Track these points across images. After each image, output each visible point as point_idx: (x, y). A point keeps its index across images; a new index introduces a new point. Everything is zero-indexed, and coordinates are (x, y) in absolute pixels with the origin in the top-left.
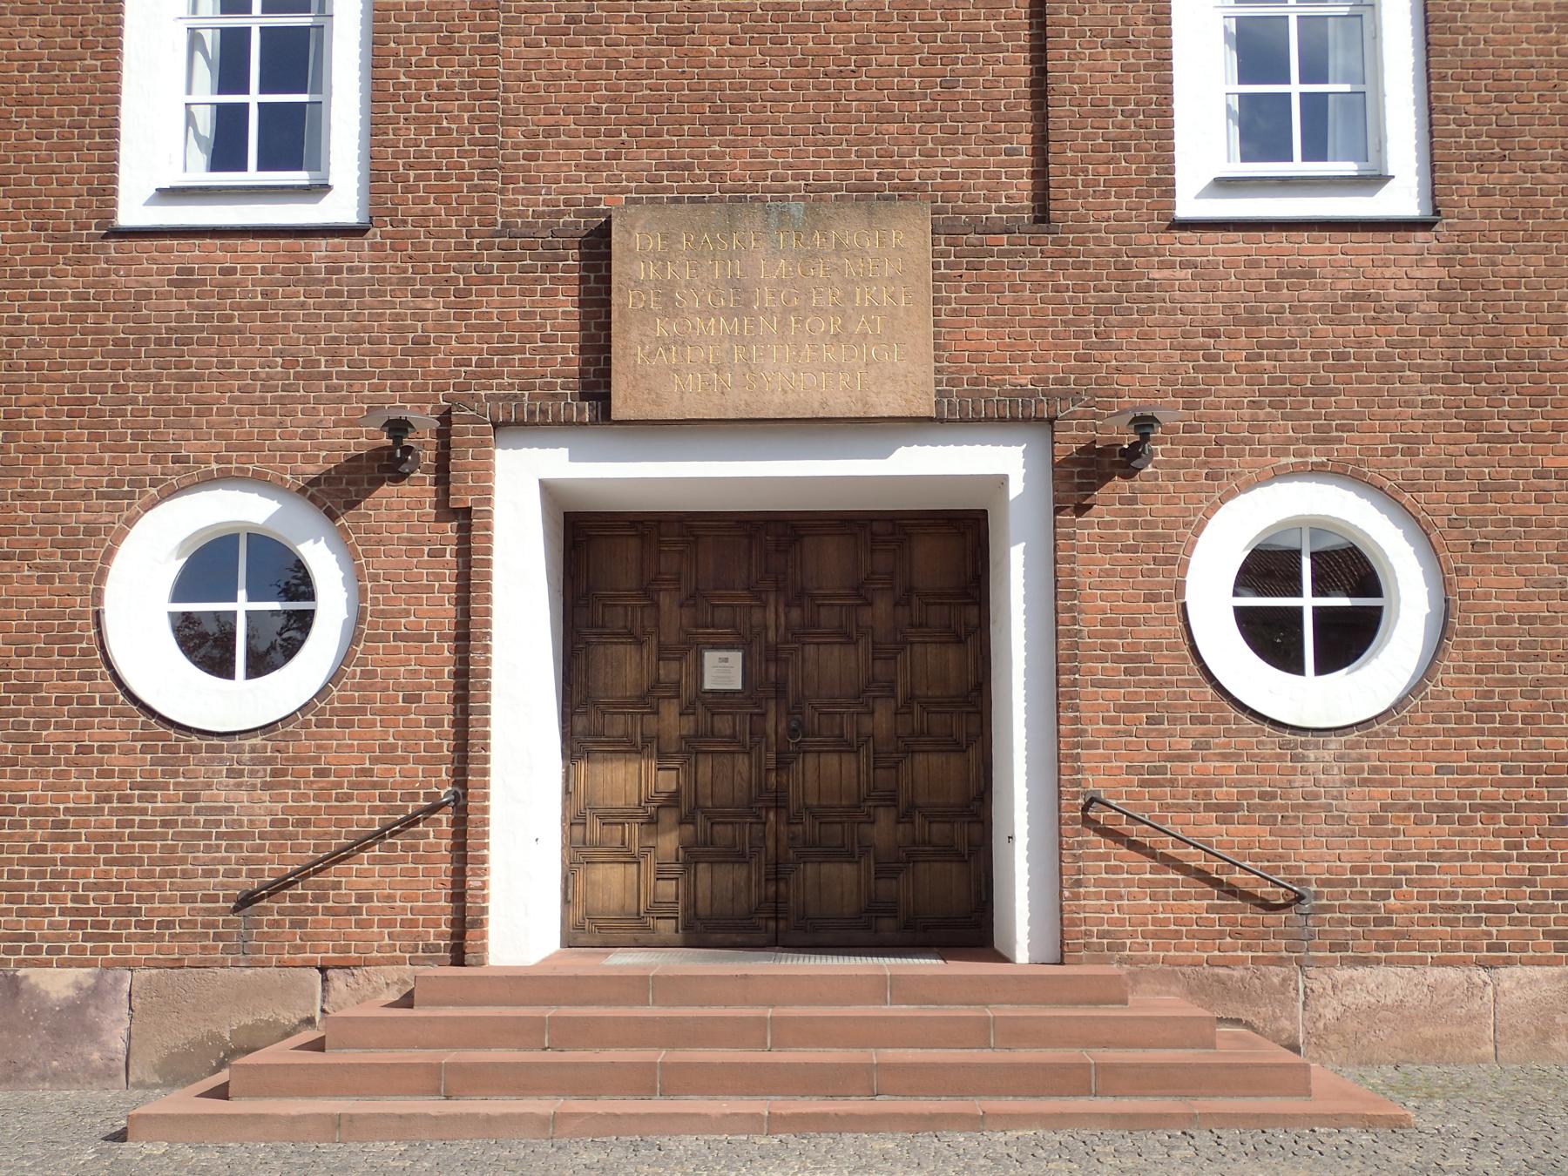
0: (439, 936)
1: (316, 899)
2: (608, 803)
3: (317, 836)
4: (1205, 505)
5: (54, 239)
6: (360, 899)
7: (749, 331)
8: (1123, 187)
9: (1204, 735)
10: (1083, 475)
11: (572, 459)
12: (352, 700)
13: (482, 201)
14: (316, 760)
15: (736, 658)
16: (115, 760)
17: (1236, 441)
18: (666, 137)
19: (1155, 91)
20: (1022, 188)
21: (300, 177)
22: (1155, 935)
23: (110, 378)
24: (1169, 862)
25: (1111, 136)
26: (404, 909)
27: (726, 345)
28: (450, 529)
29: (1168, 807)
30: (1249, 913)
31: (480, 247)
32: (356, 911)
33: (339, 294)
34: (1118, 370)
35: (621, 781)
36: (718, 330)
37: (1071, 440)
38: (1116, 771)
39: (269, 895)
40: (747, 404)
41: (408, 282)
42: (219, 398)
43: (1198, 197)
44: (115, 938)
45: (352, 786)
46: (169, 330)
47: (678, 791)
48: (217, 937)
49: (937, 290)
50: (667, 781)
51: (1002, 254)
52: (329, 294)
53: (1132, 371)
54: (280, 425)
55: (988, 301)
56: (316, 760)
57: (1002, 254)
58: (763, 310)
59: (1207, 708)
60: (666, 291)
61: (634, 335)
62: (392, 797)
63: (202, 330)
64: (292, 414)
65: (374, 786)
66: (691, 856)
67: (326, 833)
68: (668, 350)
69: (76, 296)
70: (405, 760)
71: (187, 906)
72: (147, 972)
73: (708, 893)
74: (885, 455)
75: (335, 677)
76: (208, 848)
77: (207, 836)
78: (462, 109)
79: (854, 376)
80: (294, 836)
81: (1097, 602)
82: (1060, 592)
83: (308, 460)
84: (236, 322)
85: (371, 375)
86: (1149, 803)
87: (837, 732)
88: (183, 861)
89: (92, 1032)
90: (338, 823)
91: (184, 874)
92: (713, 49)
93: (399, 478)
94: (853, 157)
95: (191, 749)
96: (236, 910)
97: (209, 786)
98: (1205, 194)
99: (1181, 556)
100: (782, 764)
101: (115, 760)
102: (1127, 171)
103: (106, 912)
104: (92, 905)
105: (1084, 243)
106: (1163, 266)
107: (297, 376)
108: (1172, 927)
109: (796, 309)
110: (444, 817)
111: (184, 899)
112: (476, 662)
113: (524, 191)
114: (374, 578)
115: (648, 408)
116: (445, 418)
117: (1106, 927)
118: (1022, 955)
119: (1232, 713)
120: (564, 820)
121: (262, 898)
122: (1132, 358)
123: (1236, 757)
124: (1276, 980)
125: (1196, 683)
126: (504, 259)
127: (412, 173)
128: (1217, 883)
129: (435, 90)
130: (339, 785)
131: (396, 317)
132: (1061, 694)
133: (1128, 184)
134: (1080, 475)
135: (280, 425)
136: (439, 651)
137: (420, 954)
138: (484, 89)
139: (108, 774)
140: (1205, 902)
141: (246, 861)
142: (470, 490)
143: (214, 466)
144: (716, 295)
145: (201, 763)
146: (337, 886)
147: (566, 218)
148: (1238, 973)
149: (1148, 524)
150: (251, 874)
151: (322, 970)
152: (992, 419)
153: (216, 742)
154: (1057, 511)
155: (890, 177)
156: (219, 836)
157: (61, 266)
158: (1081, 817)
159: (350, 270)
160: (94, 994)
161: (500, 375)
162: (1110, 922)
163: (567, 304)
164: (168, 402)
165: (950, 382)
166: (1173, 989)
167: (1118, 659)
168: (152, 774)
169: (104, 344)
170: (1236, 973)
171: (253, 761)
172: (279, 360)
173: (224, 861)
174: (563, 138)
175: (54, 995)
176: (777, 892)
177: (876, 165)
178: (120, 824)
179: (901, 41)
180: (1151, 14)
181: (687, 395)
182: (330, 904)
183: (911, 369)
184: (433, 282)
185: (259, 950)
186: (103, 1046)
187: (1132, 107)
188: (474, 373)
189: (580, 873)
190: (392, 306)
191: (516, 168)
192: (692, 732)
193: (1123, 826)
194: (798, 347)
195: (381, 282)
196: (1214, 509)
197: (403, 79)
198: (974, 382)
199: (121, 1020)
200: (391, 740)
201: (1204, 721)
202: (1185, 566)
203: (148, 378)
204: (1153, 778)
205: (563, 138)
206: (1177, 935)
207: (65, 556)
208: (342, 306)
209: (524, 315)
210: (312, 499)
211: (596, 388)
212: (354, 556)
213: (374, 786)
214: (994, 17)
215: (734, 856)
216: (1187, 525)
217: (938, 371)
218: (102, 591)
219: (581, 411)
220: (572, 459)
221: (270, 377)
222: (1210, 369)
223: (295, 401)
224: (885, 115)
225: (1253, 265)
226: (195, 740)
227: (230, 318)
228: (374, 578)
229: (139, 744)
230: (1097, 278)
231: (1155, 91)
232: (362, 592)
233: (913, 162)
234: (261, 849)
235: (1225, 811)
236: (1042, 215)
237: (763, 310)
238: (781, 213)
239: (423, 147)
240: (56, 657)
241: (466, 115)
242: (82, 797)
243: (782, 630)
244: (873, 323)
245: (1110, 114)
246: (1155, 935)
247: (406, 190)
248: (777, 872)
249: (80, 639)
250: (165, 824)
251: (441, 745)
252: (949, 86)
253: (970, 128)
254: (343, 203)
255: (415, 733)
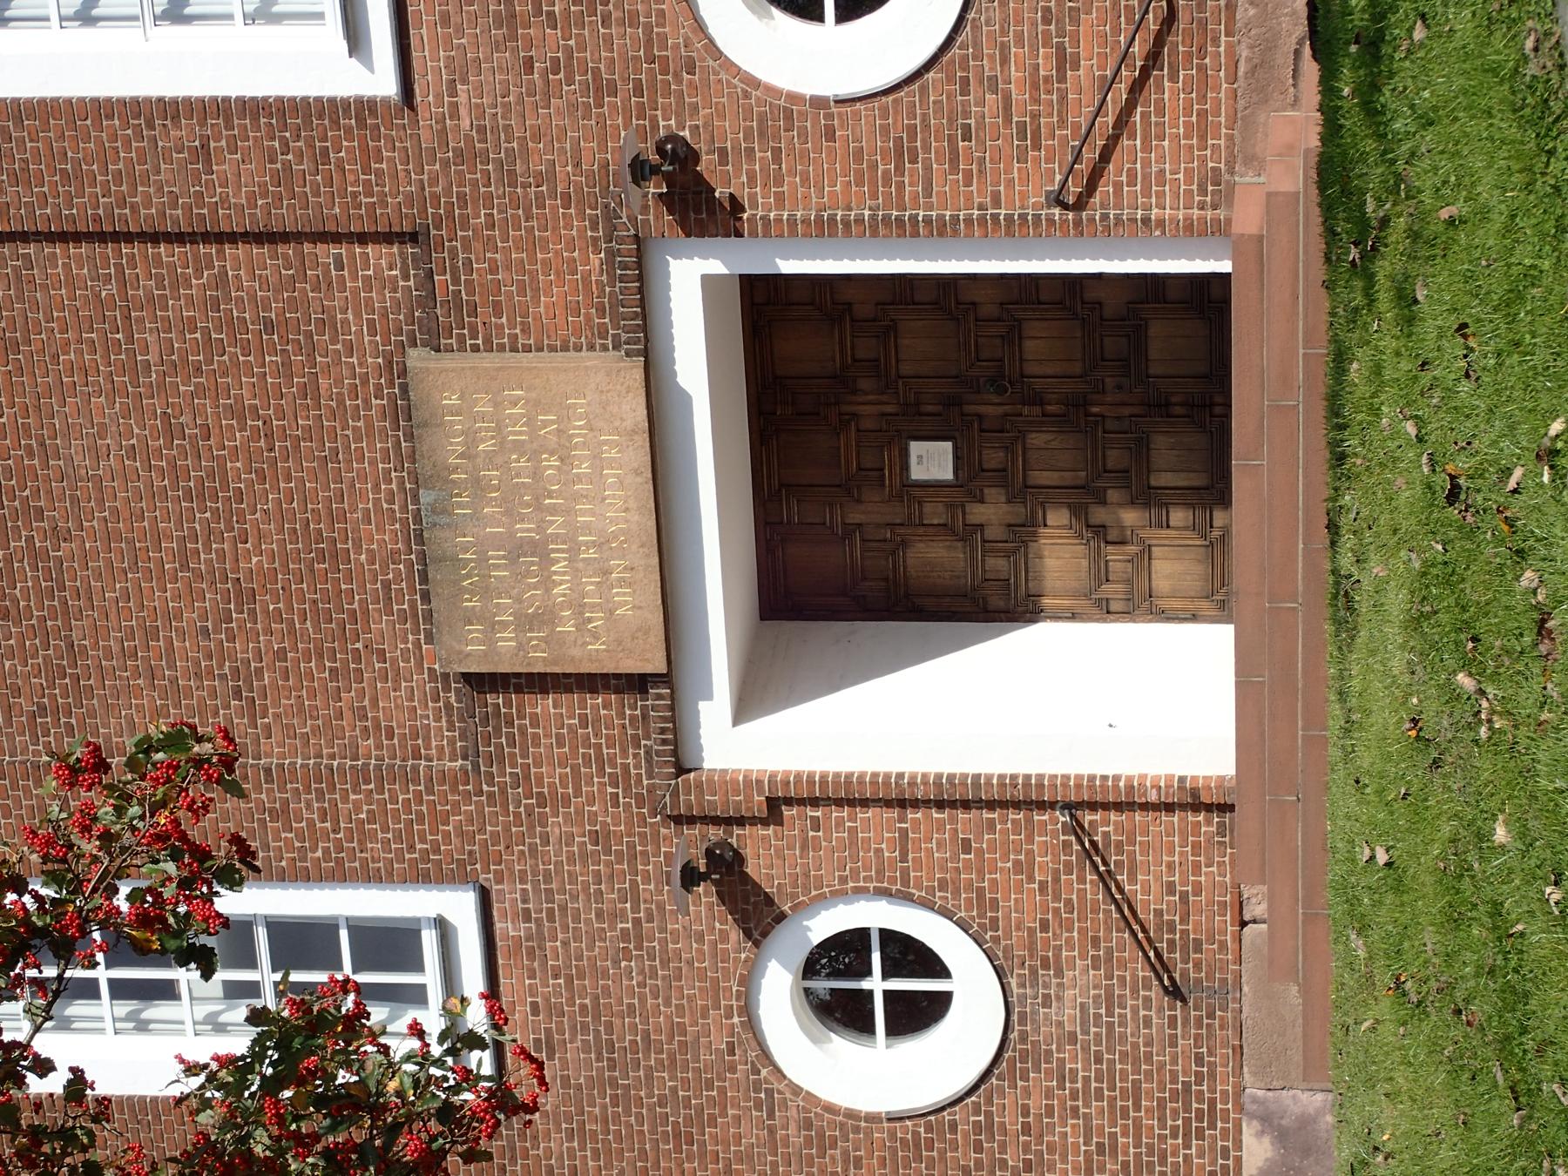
0: (1209, 822)
1: (1172, 930)
2: (1084, 575)
3: (1109, 930)
4: (723, 76)
5: (513, 1160)
6: (1172, 892)
7: (564, 543)
8: (368, 156)
9: (981, 82)
10: (700, 209)
11: (709, 697)
12: (969, 900)
13: (442, 782)
14: (1031, 931)
15: (916, 448)
16: (1036, 1103)
17: (649, 42)
18: (356, 606)
19: (255, 119)
20: (379, 256)
21: (429, 939)
22: (1203, 138)
23: (651, 1108)
24: (1123, 121)
25: (312, 167)
26: (1181, 853)
27: (581, 565)
28: (788, 812)
29: (1062, 122)
30: (1178, 41)
31: (491, 783)
32: (1184, 897)
33: (551, 912)
34: (578, 164)
35: (1059, 562)
36: (564, 573)
37: (660, 219)
38: (1024, 176)
39: (1168, 971)
40: (642, 546)
41: (533, 849)
42: (666, 1017)
43: (372, 70)
44: (1212, 1102)
45: (1057, 898)
46: (598, 1060)
47: (1069, 506)
48: (1211, 1015)
49: (502, 348)
50: (1058, 517)
51: (456, 281)
52: (551, 918)
53: (577, 150)
54: (690, 963)
55: (510, 295)
56: (1031, 931)
57: (456, 281)
58: (540, 530)
59: (950, 79)
60: (525, 622)
61: (576, 652)
62: (1068, 864)
63: (597, 1032)
64: (678, 953)
65: (1056, 880)
66: (1149, 498)
67: (1106, 922)
68: (590, 620)
69: (570, 1138)
70: (1030, 853)
71: (1180, 1042)
72: (1246, 1076)
73: (1183, 475)
74: (686, 399)
75: (946, 913)
76: (1123, 1024)
77: (1110, 1025)
78: (345, 800)
79: (605, 442)
80: (1109, 951)
81: (835, 190)
82: (824, 229)
83: (724, 937)
84: (587, 1001)
85: (634, 883)
86: (1061, 140)
87: (998, 341)
88: (1135, 1046)
89: (1306, 1122)
90: (1096, 911)
91: (1148, 1044)
92: (254, 560)
93: (739, 859)
94: (361, 424)
95: (1023, 1038)
96: (1184, 1000)
97: (1060, 1024)
98: (368, 63)
99: (782, 102)
100: (1037, 400)
101: (1036, 1103)
102: (349, 150)
103: (1187, 1109)
104: (1180, 1122)
105: (436, 198)
106: (455, 114)
107: (639, 947)
108: (1194, 119)
109: (537, 499)
110: (1088, 818)
111: (1173, 1044)
112: (926, 793)
113: (427, 739)
114: (843, 880)
115: (652, 639)
116: (678, 820)
117: (1195, 187)
118: (1225, 266)
119: (955, 51)
120: (1105, 621)
121: (1171, 978)
122: (563, 150)
123: (1004, 48)
124: (1252, 12)
125: (924, 90)
126: (501, 762)
127: (418, 846)
128: (1145, 72)
129: (328, 825)
130: (1057, 911)
131: (571, 859)
132: (943, 231)
133: (364, 149)
134: (698, 211)
135: (690, 963)
136: (916, 822)
137: (1227, 839)
138: (321, 779)
139: (1050, 1111)
140: (1167, 84)
141: (1135, 991)
142: (749, 799)
143: (736, 1020)
144: (528, 574)
145: (1037, 1031)
146: (1159, 913)
147: (453, 700)
148: (1244, 53)
149: (748, 136)
150: (1148, 987)
151: (1243, 924)
152: (642, 300)
153: (1015, 1017)
154: (739, 235)
155: (379, 387)
156: (1110, 1013)
157: (541, 1152)
158: (1075, 204)
159: (525, 901)
160: (1269, 1121)
161: (626, 767)
162: (1189, 181)
163: (546, 705)
164: (673, 1061)
165: (603, 334)
166: (1262, 118)
167: (900, 170)
168: (1049, 1072)
169: (616, 1116)
170: (1244, 54)
171: (1034, 984)
172: (623, 964)
173: (1135, 1010)
174: (366, 703)
175: (1269, 1154)
176: (1181, 405)
177: (367, 402)
178: (1100, 1097)
179: (225, 374)
180: (168, 122)
181: (635, 602)
182: (1177, 918)
183: (593, 386)
184: (531, 827)
185: (1224, 981)
186: (1320, 1112)
187: (277, 144)
188: (624, 790)
189: (1163, 604)
190: (559, 864)
191: (403, 746)
192: (1003, 491)
193: (1083, 167)
194: (577, 497)
195: (535, 873)
196: (729, 65)
197: (319, 854)
198: (601, 312)
199: (1294, 1097)
200: (1010, 864)
201: (965, 82)
202: (794, 98)
203: (649, 1077)
204: (1030, 135)
205: (366, 703)
206: (1202, 114)
207: (834, 1146)
208: (563, 909)
209: (560, 744)
210: (765, 935)
211: (638, 684)
212: (822, 897)
213: (1056, 880)
214: (187, 280)
215: (1141, 450)
216: (747, 95)
217: (591, 348)
218: (867, 1114)
219: (659, 697)
220: (709, 697)
221: (642, 972)
222: (569, 65)
223: (664, 950)
224: (310, 391)
225: (446, 19)
226: (1014, 1036)
227: (583, 1007)
228: (843, 880)
229: (1020, 1083)
230: (475, 183)
231: (255, 119)
232: (859, 891)
233: (360, 365)
234: (1122, 979)
235: (1065, 62)
236: (413, 238)
237: (540, 530)
238: (433, 512)
239: (390, 836)
240: (935, 1153)
241: (352, 797)
242: (1073, 1132)
243: (884, 398)
244: (545, 424)
245: (287, 166)
246: (1203, 138)
247: (437, 851)
248: (1159, 407)
249: (916, 1134)
250: (1099, 1060)
251: (1014, 821)
252: (269, 326)
253: (315, 305)
254: (460, 906)
255: (1002, 844)
